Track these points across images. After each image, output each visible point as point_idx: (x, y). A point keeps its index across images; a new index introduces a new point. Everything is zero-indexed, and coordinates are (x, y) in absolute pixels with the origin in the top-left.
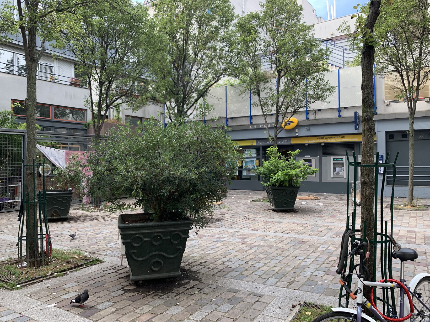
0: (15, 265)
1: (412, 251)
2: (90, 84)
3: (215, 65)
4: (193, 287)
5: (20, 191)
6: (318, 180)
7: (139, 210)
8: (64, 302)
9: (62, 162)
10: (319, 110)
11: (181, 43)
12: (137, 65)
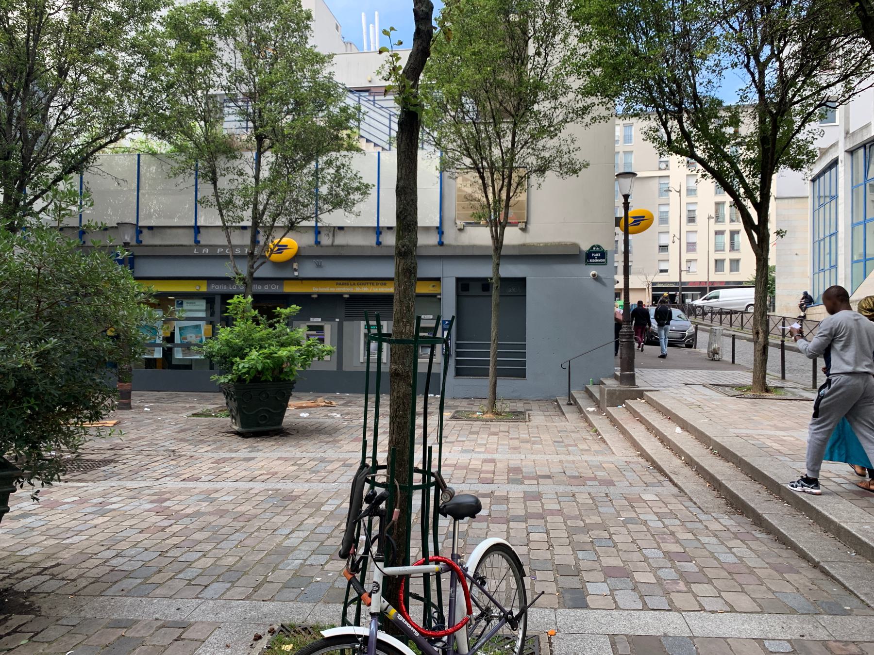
1: (472, 500)
3: (109, 102)
4: (15, 631)
6: (334, 368)
10: (341, 228)
11: (21, 36)
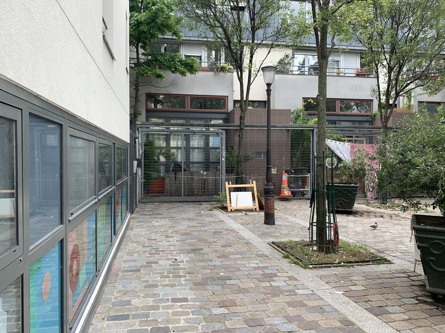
0: (307, 247)
2: (377, 72)
5: (309, 181)
7: (438, 212)
8: (351, 293)
9: (347, 155)
12: (437, 40)
